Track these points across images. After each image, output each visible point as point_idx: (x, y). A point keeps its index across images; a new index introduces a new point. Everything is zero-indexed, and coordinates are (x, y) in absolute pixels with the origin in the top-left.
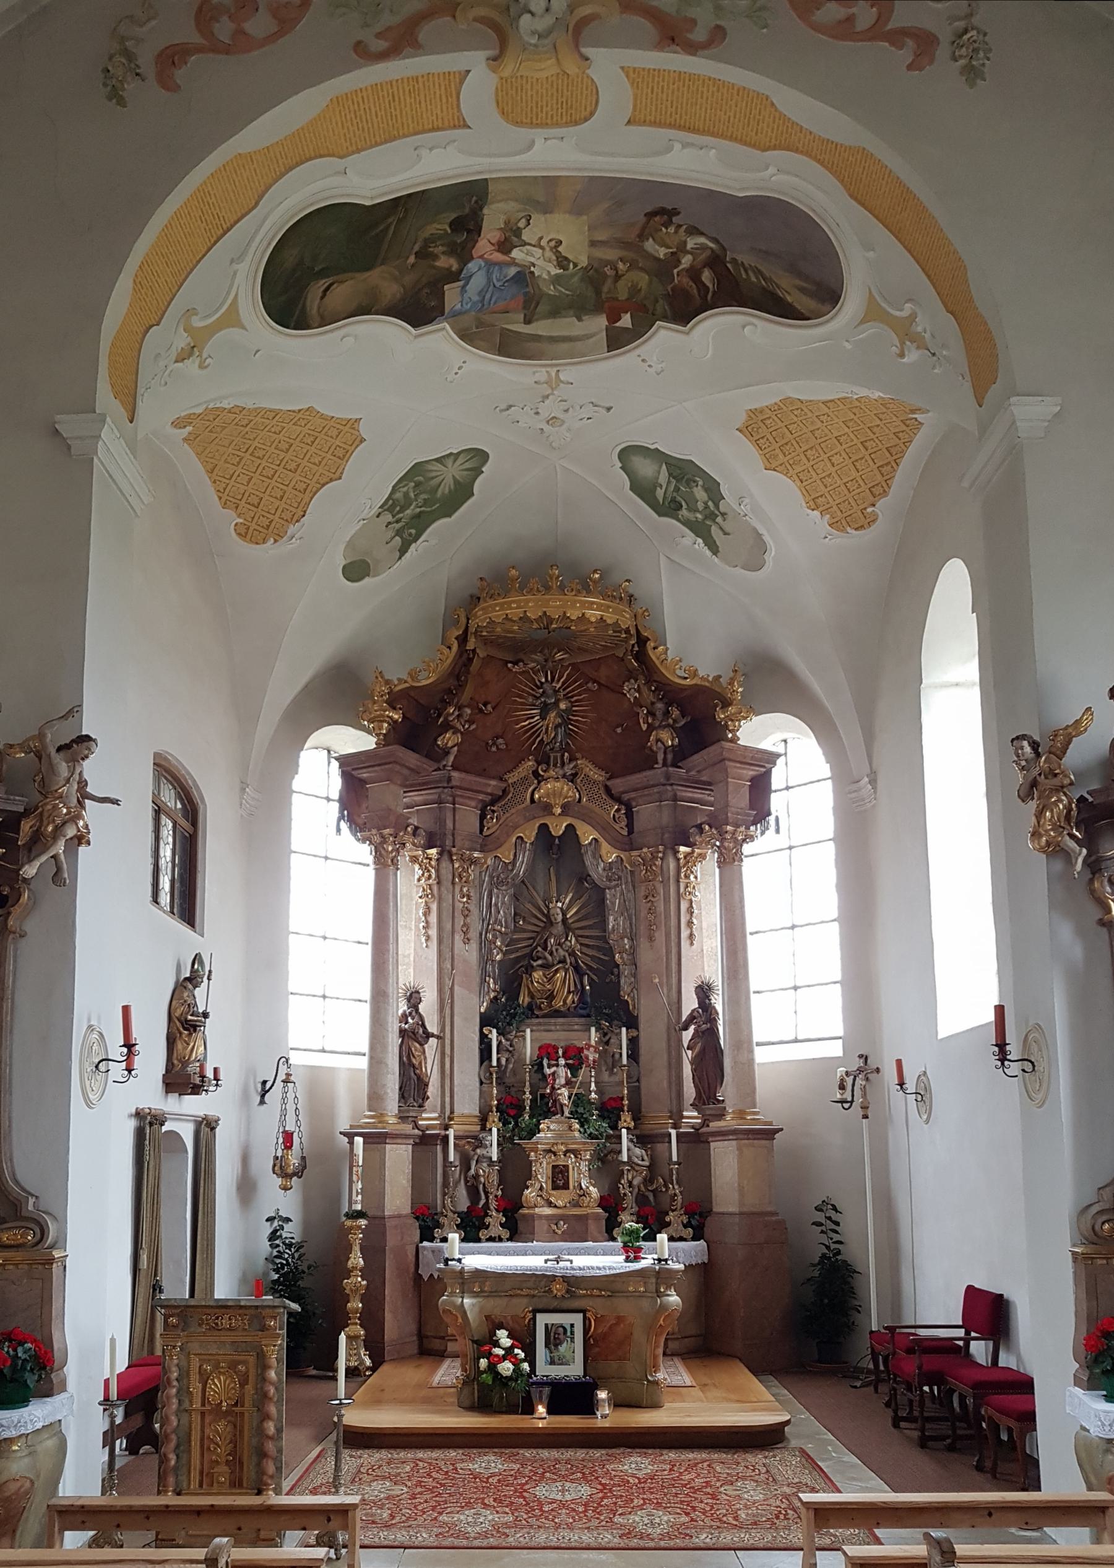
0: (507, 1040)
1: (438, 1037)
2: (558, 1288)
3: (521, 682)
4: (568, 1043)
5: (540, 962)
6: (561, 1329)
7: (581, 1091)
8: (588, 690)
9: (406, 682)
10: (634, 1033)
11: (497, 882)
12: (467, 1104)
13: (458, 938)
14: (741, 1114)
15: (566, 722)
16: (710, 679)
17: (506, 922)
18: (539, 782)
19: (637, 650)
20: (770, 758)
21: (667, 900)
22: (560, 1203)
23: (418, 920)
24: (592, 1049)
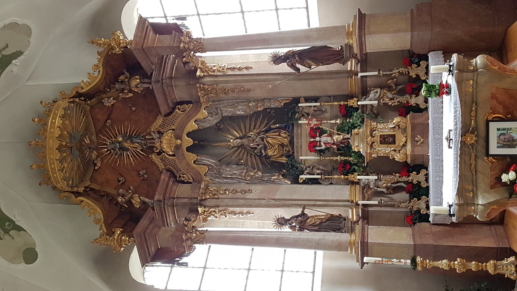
0: (306, 169)
1: (304, 208)
2: (470, 139)
3: (107, 162)
4: (308, 136)
5: (263, 151)
6: (501, 137)
7: (335, 128)
8: (111, 124)
9: (101, 226)
10: (302, 99)
11: (219, 175)
12: (344, 192)
13: (248, 196)
14: (349, 34)
15: (130, 137)
16: (99, 57)
17: (240, 170)
18: (164, 152)
19: (83, 97)
20: (142, 21)
21: (227, 82)
22: (404, 140)
23: (239, 218)
24: (310, 122)
